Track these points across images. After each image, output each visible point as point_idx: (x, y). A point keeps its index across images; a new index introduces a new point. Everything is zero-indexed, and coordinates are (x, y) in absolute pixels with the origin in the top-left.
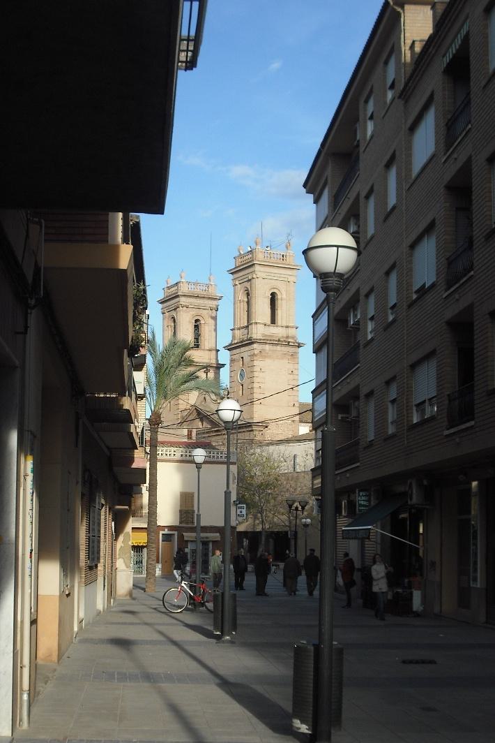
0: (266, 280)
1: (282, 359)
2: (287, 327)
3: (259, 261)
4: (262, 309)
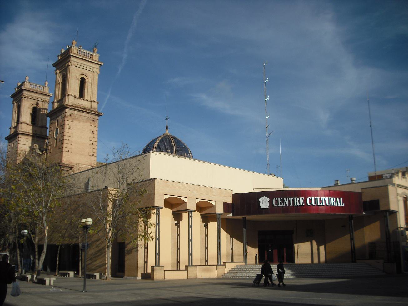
0: (76, 68)
1: (86, 122)
2: (91, 101)
3: (73, 53)
4: (73, 87)
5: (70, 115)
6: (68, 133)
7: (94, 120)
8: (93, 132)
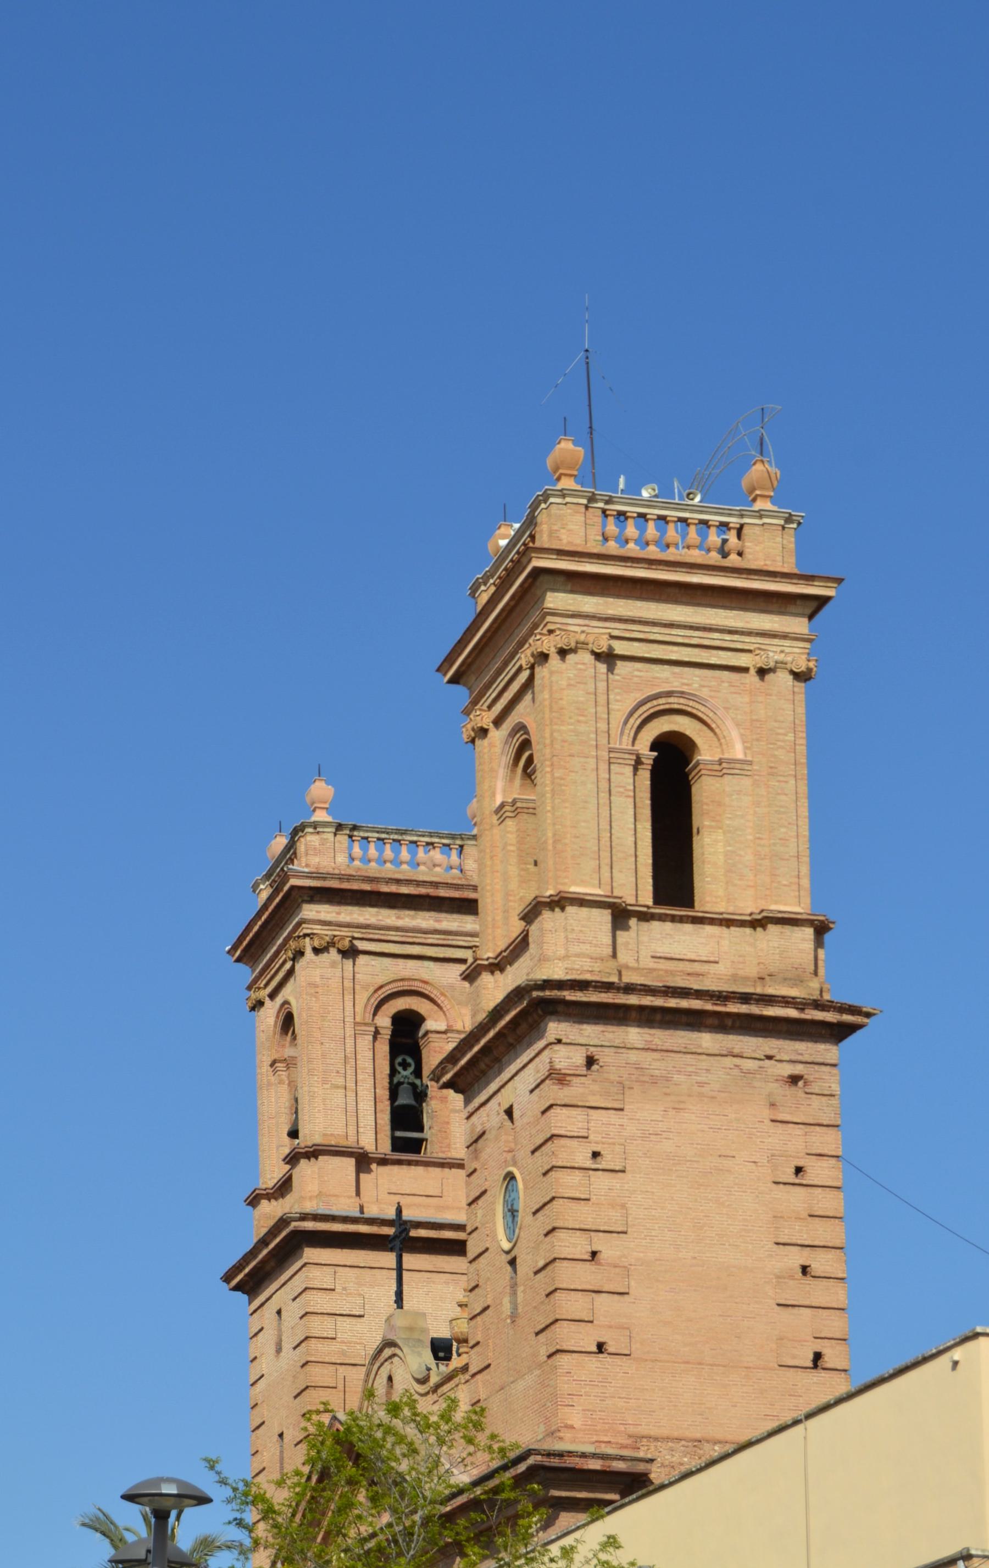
5: (590, 1061)
6: (582, 1206)
7: (798, 1069)
8: (799, 1170)
